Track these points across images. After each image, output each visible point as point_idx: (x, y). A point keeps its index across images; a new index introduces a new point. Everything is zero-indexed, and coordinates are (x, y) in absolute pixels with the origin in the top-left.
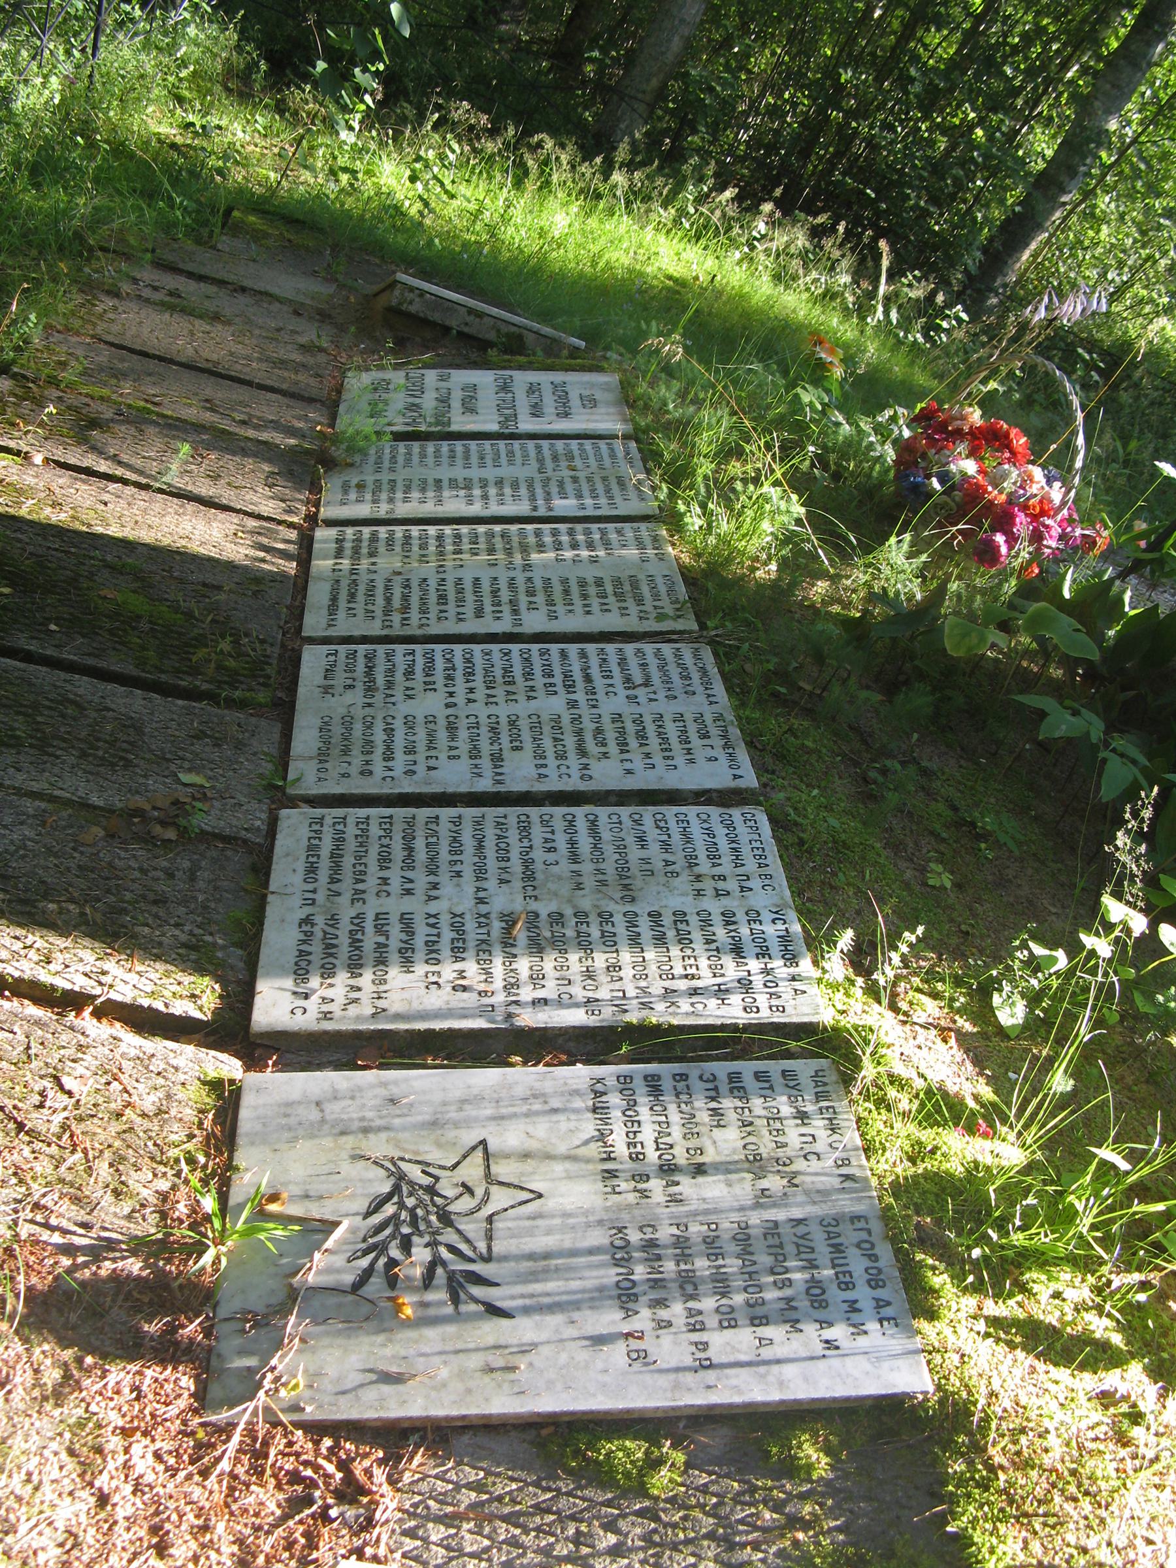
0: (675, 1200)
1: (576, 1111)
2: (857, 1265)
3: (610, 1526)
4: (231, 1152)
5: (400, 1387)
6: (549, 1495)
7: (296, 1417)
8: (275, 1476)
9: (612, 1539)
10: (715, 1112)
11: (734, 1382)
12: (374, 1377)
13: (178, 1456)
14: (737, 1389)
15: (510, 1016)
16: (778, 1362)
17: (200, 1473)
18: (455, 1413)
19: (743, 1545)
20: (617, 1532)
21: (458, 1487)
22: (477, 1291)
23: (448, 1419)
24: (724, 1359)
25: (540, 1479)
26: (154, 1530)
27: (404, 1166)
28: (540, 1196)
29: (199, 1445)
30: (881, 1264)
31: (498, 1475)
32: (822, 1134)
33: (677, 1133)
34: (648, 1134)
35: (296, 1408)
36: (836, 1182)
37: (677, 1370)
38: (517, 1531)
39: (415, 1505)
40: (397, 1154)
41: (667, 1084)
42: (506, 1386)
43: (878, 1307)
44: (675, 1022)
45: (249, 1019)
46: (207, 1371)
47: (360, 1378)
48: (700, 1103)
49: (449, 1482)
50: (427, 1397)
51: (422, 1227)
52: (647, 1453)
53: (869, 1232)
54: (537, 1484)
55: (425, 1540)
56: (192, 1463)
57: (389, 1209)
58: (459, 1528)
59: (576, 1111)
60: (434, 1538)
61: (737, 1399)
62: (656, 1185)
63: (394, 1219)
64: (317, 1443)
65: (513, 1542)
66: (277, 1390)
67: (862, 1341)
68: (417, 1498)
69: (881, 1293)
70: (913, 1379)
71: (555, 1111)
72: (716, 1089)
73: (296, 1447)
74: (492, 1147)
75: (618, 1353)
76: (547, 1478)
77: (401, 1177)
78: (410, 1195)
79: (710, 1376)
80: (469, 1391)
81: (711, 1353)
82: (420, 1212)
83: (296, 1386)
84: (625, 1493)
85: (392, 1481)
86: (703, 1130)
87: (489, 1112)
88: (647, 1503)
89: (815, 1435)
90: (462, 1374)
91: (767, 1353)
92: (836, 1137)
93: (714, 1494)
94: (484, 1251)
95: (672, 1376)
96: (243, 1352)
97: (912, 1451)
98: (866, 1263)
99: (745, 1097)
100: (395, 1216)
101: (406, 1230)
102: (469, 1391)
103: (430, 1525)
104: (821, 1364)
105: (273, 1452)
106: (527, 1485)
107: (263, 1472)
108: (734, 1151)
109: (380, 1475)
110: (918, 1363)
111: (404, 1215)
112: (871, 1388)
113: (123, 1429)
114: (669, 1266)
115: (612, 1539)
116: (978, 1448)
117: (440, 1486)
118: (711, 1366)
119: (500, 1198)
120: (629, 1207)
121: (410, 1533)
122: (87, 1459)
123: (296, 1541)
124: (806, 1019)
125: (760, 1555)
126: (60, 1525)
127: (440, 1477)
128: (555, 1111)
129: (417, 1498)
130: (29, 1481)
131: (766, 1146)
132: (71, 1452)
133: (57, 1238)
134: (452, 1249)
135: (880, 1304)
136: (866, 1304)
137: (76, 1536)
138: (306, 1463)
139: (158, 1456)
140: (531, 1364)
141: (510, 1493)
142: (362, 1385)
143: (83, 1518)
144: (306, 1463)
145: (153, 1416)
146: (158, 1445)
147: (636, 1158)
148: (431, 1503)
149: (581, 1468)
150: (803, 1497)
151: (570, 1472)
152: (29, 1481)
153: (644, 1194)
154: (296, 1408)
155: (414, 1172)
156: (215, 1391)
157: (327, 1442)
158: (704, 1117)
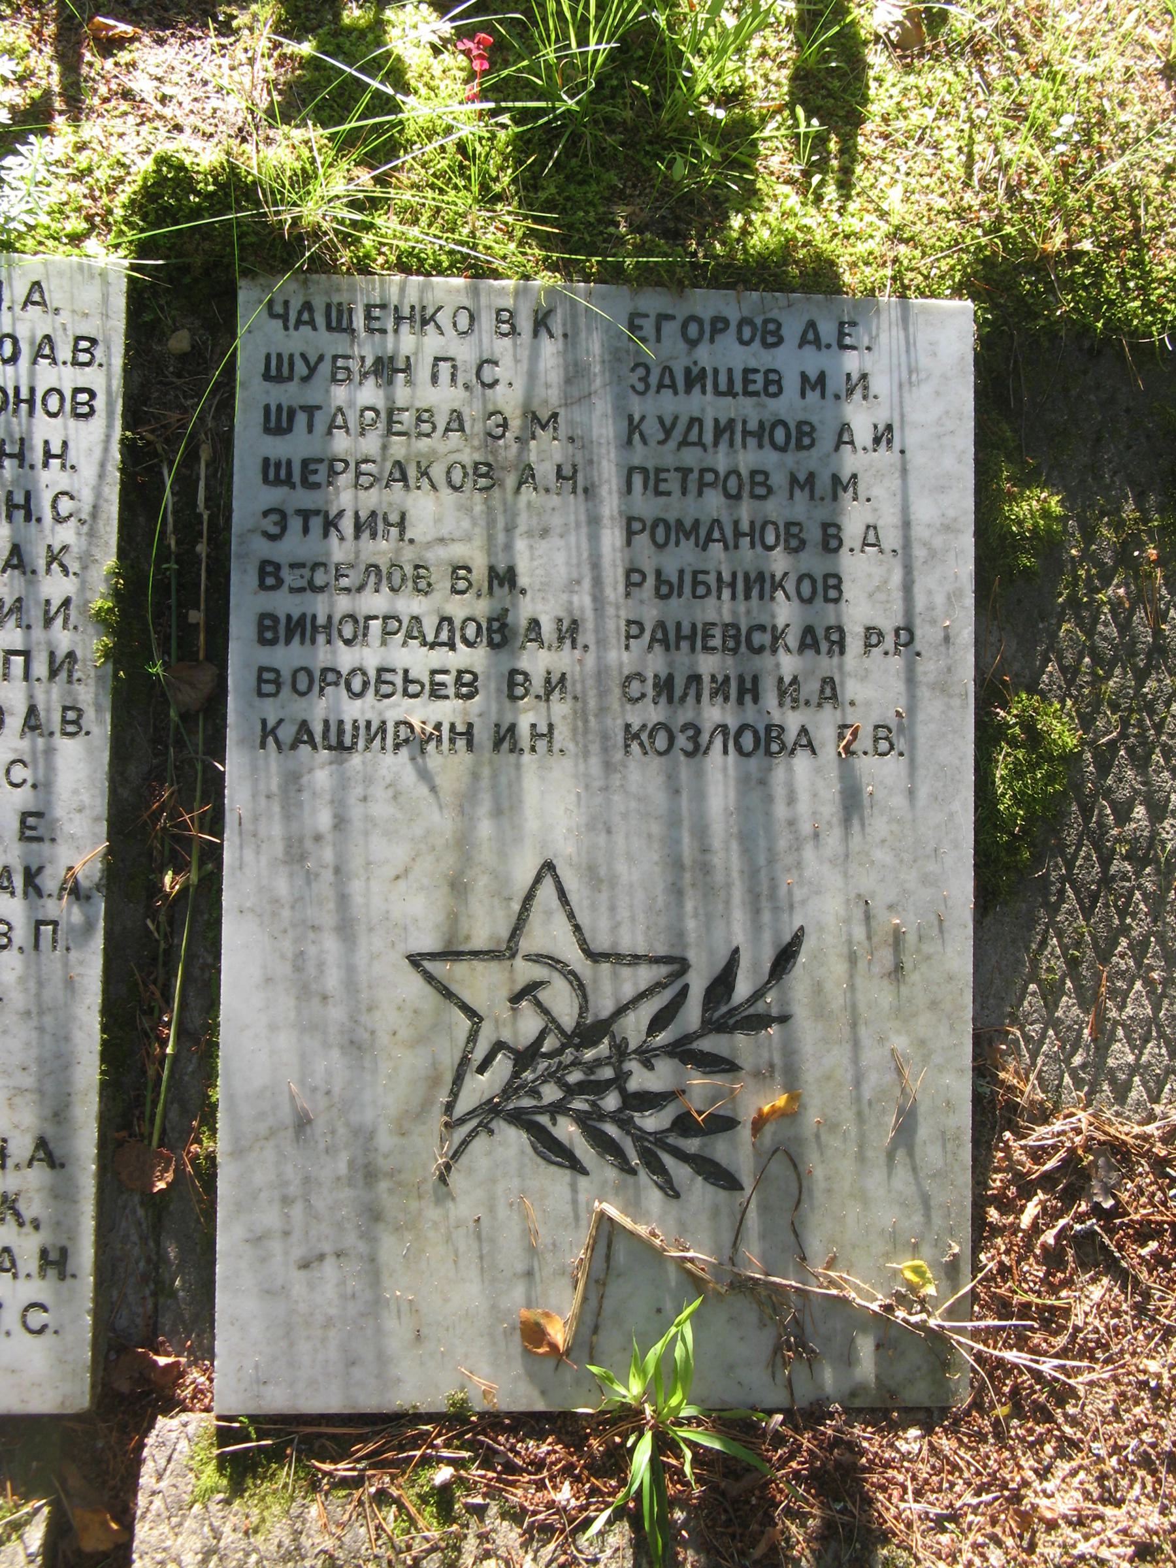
0: (569, 632)
1: (343, 784)
2: (729, 355)
3: (1123, 814)
4: (419, 1418)
5: (922, 1109)
6: (1070, 893)
8: (1054, 1290)
9: (1140, 811)
10: (366, 525)
11: (939, 599)
12: (900, 1155)
13: (1041, 1441)
14: (952, 598)
15: (76, 892)
16: (906, 525)
17: (1061, 1403)
20: (1130, 805)
21: (1052, 1022)
22: (743, 989)
24: (898, 606)
25: (1046, 904)
27: (467, 1101)
28: (548, 867)
29: (1018, 1411)
30: (733, 315)
31: (1035, 963)
32: (432, 344)
33: (409, 605)
34: (417, 660)
35: (951, 1271)
36: (550, 349)
37: (911, 680)
38: (1124, 942)
39: (1078, 1083)
40: (437, 1119)
41: (284, 604)
42: (927, 948)
43: (817, 342)
44: (110, 561)
45: (55, 1419)
46: (886, 1412)
47: (902, 1173)
48: (339, 551)
49: (1044, 1035)
50: (941, 1069)
51: (607, 1073)
52: (1013, 743)
53: (663, 318)
54: (1054, 909)
55: (1134, 1069)
56: (1050, 1418)
57: (567, 1130)
58: (1116, 1023)
59: (343, 784)
60: (1131, 1058)
62: (537, 662)
63: (588, 1123)
64: (997, 1231)
65: (1139, 949)
66: (922, 1301)
67: (880, 384)
68: (1067, 1079)
69: (792, 329)
70: (952, 327)
71: (340, 822)
72: (306, 515)
74: (427, 942)
75: (880, 773)
76: (1046, 893)
77: (490, 1112)
78: (535, 1093)
79: (926, 634)
80: (934, 1005)
81: (888, 623)
82: (575, 1077)
83: (917, 1270)
85: (1043, 1116)
86: (408, 556)
87: (331, 944)
90: (902, 1013)
91: (891, 538)
92: (443, 318)
94: (663, 970)
95: (924, 693)
96: (848, 1359)
97: (1055, 358)
98: (728, 339)
99: (332, 466)
100: (581, 1119)
101: (611, 1102)
102: (934, 1005)
103: (1111, 1062)
104: (917, 459)
106: (1052, 923)
107: (1051, 1309)
108: (460, 507)
109: (1041, 1134)
110: (924, 310)
111: (579, 1104)
112: (962, 396)
114: (708, 665)
115: (1140, 811)
116: (1040, 264)
118: (910, 630)
119: (550, 933)
120: (581, 714)
121: (1121, 1093)
123: (1154, 1254)
124: (120, 303)
128: (340, 822)
129: (1067, 1079)
131: (460, 450)
134: (658, 1023)
135: (810, 337)
136: (812, 361)
139: (1044, 1473)
140: (891, 907)
141: (1065, 948)
146: (1029, 1475)
147: (467, 685)
148: (1077, 1060)
149: (1032, 845)
150: (1089, 535)
151: (1038, 860)
153: (555, 685)
155: (481, 1087)
156: (918, 1393)
157: (993, 1214)
158: (380, 549)
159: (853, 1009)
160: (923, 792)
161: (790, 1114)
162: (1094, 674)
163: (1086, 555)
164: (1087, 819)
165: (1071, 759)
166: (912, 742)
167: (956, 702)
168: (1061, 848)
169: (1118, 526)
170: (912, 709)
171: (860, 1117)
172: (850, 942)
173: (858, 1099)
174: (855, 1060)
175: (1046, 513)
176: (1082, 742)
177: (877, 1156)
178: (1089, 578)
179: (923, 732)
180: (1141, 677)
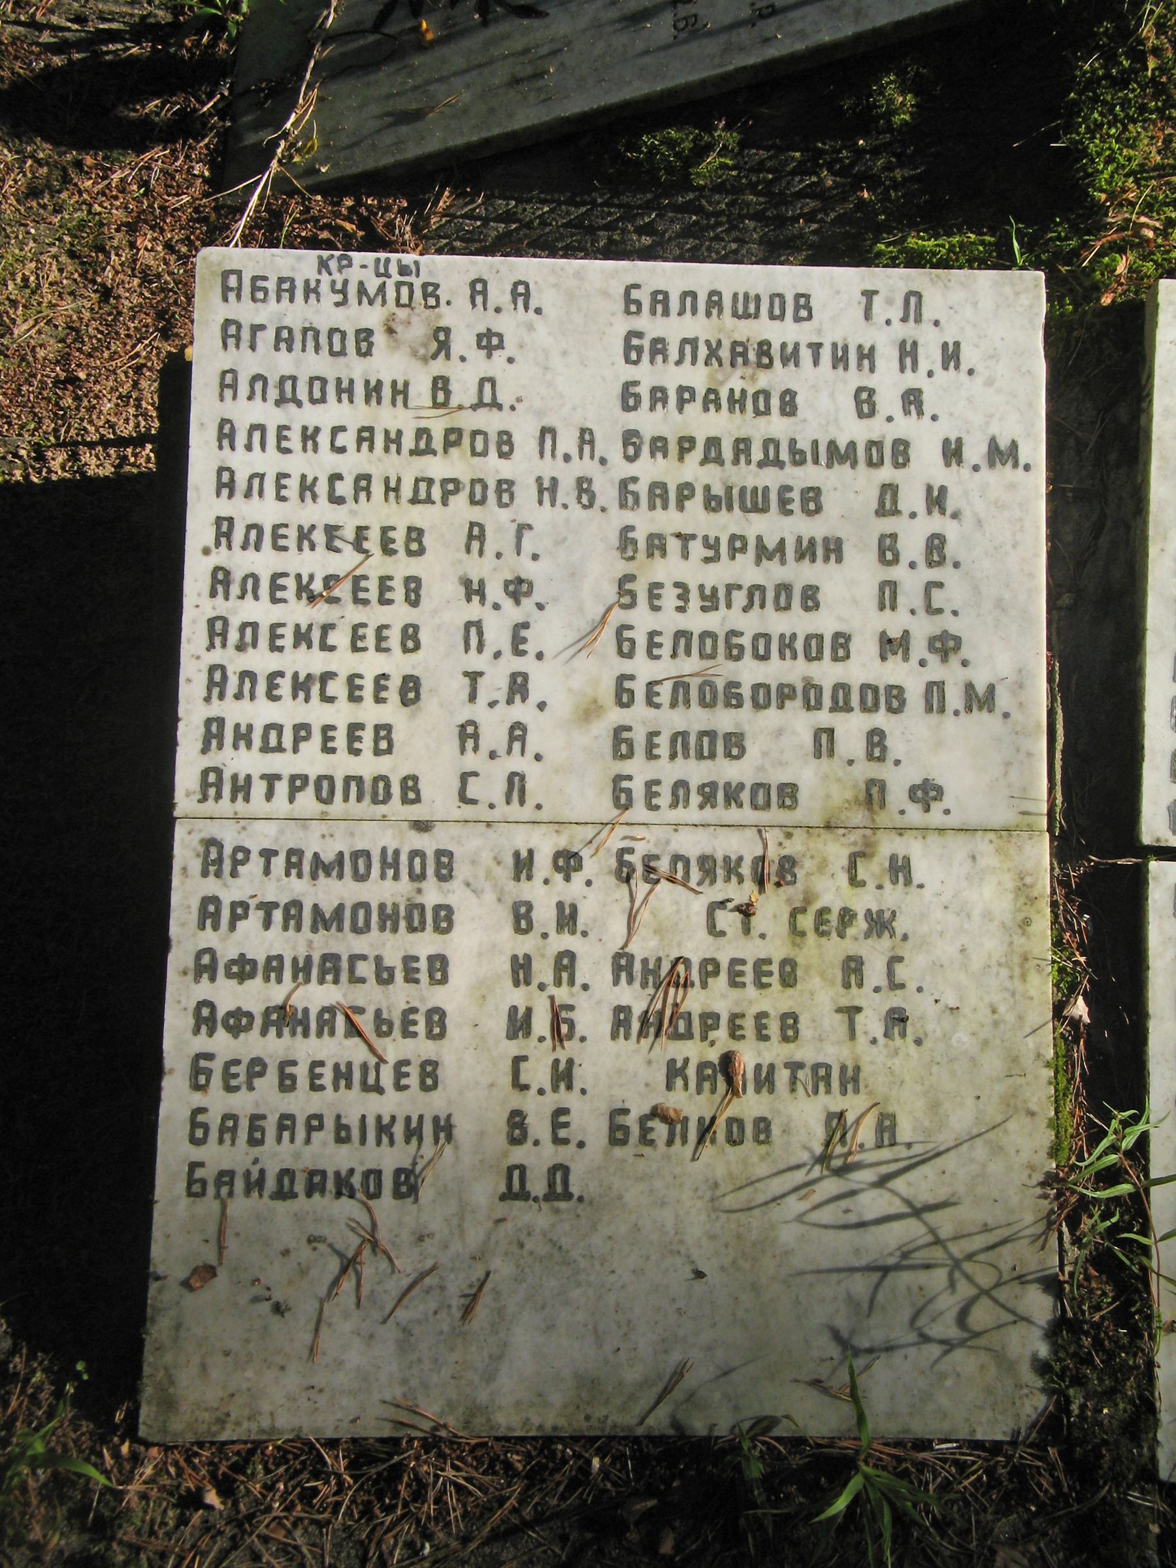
5: (419, 125)
7: (310, 181)
11: (798, 26)
12: (390, 119)
14: (802, 34)
18: (475, 138)
19: (795, 219)
21: (486, 221)
23: (470, 147)
26: (161, 315)
31: (529, 201)
47: (375, 124)
61: (799, 46)
66: (291, 157)
73: (314, 212)
75: (662, 28)
79: (769, 26)
84: (668, 190)
88: (691, 196)
89: (901, 73)
93: (769, 171)
95: (722, 39)
102: (492, 111)
105: (288, 221)
106: (560, 203)
113: (127, 224)
117: (468, 225)
122: (88, 254)
125: (814, 226)
126: (60, 321)
127: (470, 216)
130: (26, 286)
132: (72, 254)
133: (46, 37)
137: (77, 330)
138: (326, 227)
139: (169, 246)
142: (379, 131)
143: (87, 315)
144: (326, 227)
145: (162, 208)
152: (26, 286)
154: (312, 171)
159: (491, 62)
160: (647, 59)
161: (422, 47)
162: (758, 182)
163: (860, 152)
164: (640, 207)
165: (685, 184)
166: (685, 41)
167: (717, 61)
168: (616, 194)
169: (889, 168)
170: (711, 34)
171: (415, 88)
172: (537, 46)
173: (428, 83)
174: (455, 74)
175: (892, 113)
176: (701, 189)
177: (390, 106)
178: (840, 160)
179: (694, 47)
180: (758, 217)
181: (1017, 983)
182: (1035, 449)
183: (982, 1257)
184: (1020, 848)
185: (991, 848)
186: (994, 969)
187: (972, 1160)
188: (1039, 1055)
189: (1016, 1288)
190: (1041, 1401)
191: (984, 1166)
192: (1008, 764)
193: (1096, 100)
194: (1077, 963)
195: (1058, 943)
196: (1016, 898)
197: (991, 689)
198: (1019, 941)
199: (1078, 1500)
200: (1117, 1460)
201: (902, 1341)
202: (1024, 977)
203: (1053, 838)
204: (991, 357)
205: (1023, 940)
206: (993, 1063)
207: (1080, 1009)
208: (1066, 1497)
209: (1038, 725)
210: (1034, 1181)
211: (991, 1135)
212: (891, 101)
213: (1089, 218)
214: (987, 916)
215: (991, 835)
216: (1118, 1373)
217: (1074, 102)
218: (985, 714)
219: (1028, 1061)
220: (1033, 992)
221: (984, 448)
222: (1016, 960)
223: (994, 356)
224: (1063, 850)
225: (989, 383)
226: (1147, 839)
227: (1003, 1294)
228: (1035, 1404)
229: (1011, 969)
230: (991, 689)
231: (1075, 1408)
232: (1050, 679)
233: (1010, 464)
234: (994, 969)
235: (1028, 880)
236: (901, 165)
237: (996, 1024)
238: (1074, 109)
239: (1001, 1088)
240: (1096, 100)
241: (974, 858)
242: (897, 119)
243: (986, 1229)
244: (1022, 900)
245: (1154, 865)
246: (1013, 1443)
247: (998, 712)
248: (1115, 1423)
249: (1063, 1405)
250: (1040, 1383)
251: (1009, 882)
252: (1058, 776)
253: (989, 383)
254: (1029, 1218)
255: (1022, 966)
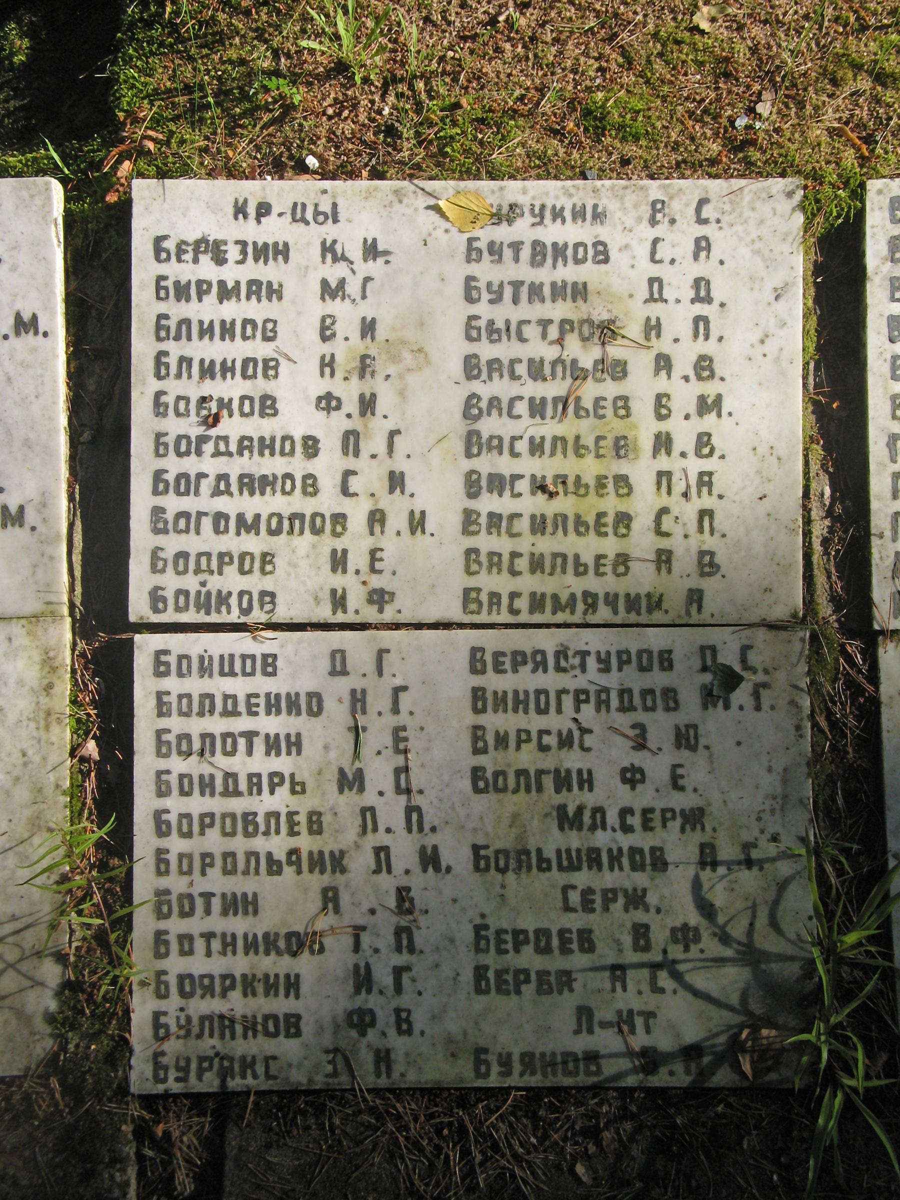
89: (19, 22)
175: (12, 54)
181: (42, 732)
182: (56, 322)
183: (10, 940)
184: (46, 630)
185: (23, 632)
186: (25, 723)
187: (5, 868)
188: (58, 786)
189: (35, 960)
190: (49, 1044)
191: (14, 872)
192: (35, 566)
193: (132, 38)
194: (89, 715)
195: (74, 702)
196: (42, 669)
197: (21, 508)
198: (44, 700)
199: (70, 1113)
200: (97, 1083)
201: (787, 934)
202: (47, 728)
203: (74, 621)
204: (14, 248)
205: (47, 700)
206: (23, 794)
207: (91, 748)
208: (62, 1111)
209: (58, 535)
210: (52, 881)
211: (20, 848)
212: (12, 44)
213: (111, 131)
214: (20, 683)
215: (24, 621)
216: (103, 1018)
217: (121, 40)
218: (17, 529)
219: (49, 791)
220: (54, 739)
221: (11, 321)
222: (42, 715)
223: (15, 248)
224: (81, 629)
225: (14, 269)
226: (132, 618)
227: (25, 967)
228: (45, 1045)
229: (38, 722)
230: (21, 508)
231: (71, 1047)
232: (71, 498)
233: (32, 332)
234: (25, 723)
235: (51, 654)
236: (15, 97)
237: (25, 764)
238: (118, 47)
239: (28, 813)
240: (132, 38)
241: (10, 639)
242: (15, 59)
243: (14, 918)
244: (47, 669)
245: (137, 637)
246: (25, 1076)
247: (27, 526)
248: (100, 1056)
249: (64, 1048)
250: (48, 1030)
251: (37, 656)
252: (78, 573)
253: (14, 269)
254: (47, 908)
255: (46, 719)
